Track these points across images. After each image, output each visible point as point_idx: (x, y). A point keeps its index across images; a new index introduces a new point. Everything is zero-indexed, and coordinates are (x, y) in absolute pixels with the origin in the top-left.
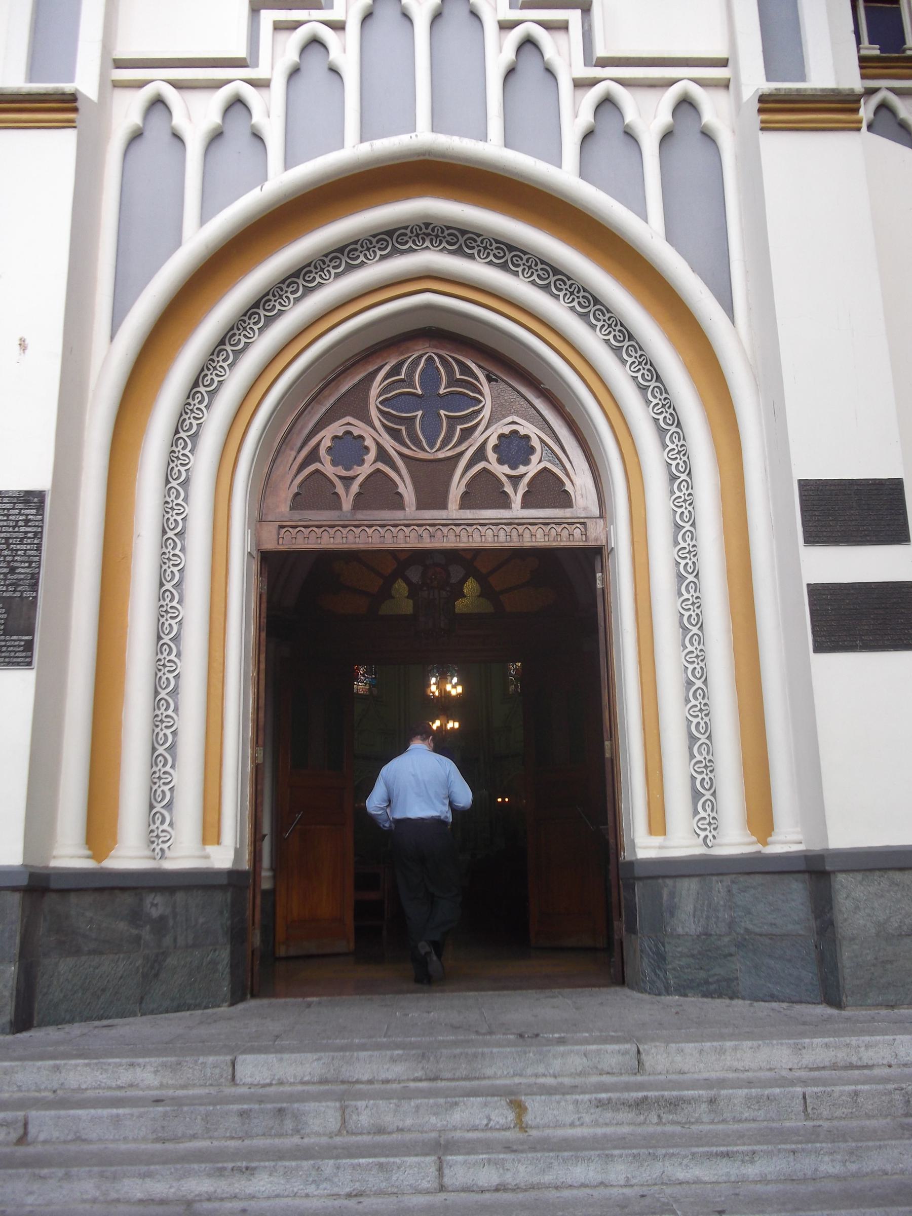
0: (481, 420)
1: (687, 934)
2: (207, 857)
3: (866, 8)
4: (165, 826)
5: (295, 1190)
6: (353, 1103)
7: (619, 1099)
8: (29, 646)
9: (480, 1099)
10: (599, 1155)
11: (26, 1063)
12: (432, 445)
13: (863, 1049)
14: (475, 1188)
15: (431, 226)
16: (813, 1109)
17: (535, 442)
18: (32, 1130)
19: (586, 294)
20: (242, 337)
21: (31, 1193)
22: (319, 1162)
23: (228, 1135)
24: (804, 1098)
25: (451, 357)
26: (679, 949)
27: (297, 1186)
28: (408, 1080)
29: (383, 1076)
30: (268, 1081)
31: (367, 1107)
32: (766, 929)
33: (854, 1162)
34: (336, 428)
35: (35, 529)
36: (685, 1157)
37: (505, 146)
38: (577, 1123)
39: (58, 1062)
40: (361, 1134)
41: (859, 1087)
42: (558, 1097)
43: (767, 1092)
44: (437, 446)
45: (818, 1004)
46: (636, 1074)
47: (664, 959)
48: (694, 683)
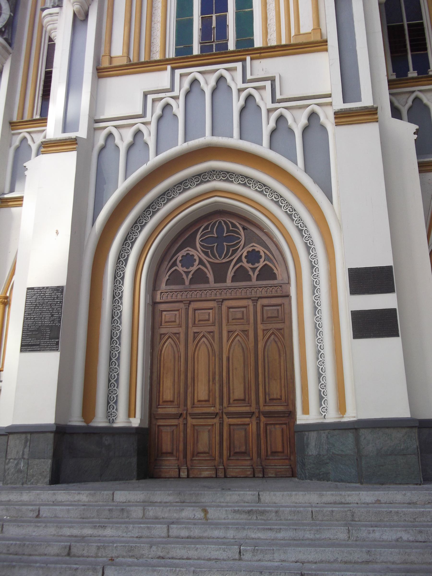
0: (240, 246)
1: (312, 455)
2: (130, 422)
3: (412, 55)
4: (114, 410)
5: (119, 534)
6: (147, 508)
7: (242, 510)
8: (57, 343)
9: (192, 508)
10: (224, 527)
11: (45, 491)
12: (220, 257)
13: (347, 496)
14: (180, 537)
15: (215, 171)
16: (315, 516)
17: (262, 254)
18: (41, 513)
19: (277, 193)
20: (144, 220)
21: (34, 532)
22: (127, 525)
23: (105, 517)
24: (312, 512)
25: (228, 221)
26: (310, 461)
27: (120, 533)
28: (174, 502)
29: (165, 500)
30: (125, 501)
31: (152, 509)
32: (340, 452)
33: (318, 534)
34: (183, 252)
35: (60, 300)
36: (255, 529)
37: (241, 139)
38: (226, 518)
39: (55, 492)
40: (150, 519)
41: (334, 509)
42: (220, 508)
43: (298, 509)
44: (223, 257)
45: (357, 483)
46: (257, 503)
47: (304, 465)
48: (321, 352)
